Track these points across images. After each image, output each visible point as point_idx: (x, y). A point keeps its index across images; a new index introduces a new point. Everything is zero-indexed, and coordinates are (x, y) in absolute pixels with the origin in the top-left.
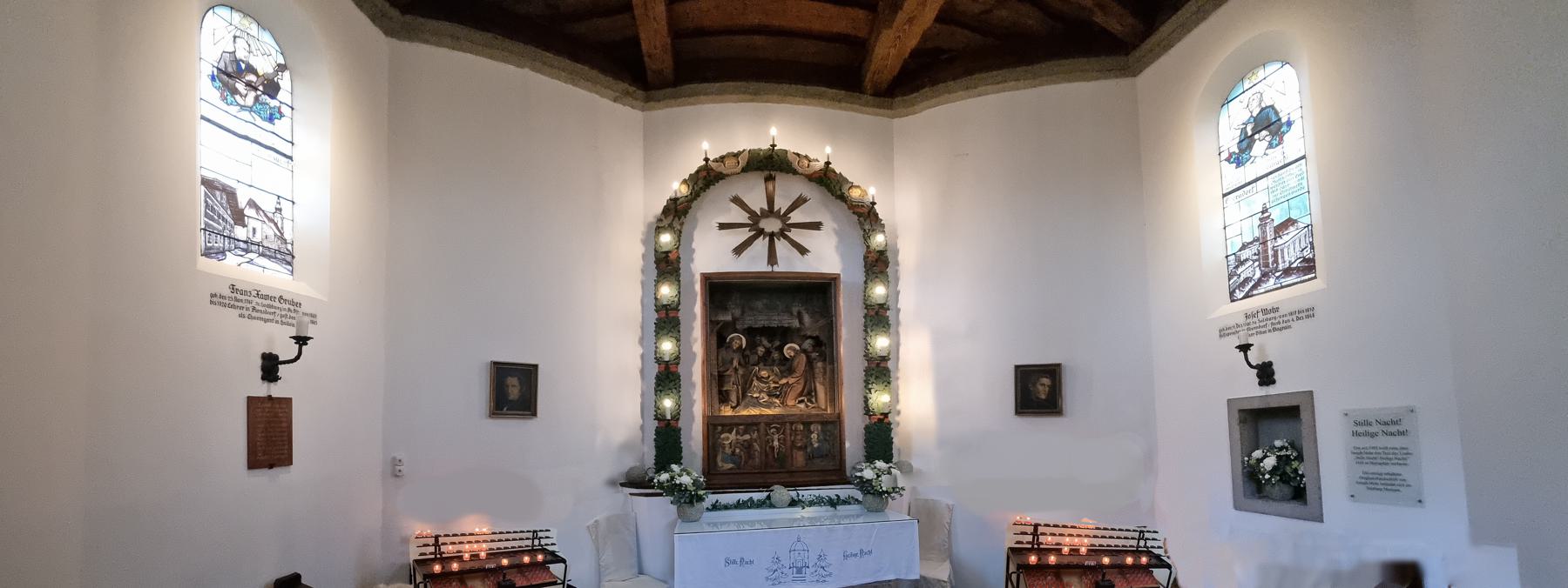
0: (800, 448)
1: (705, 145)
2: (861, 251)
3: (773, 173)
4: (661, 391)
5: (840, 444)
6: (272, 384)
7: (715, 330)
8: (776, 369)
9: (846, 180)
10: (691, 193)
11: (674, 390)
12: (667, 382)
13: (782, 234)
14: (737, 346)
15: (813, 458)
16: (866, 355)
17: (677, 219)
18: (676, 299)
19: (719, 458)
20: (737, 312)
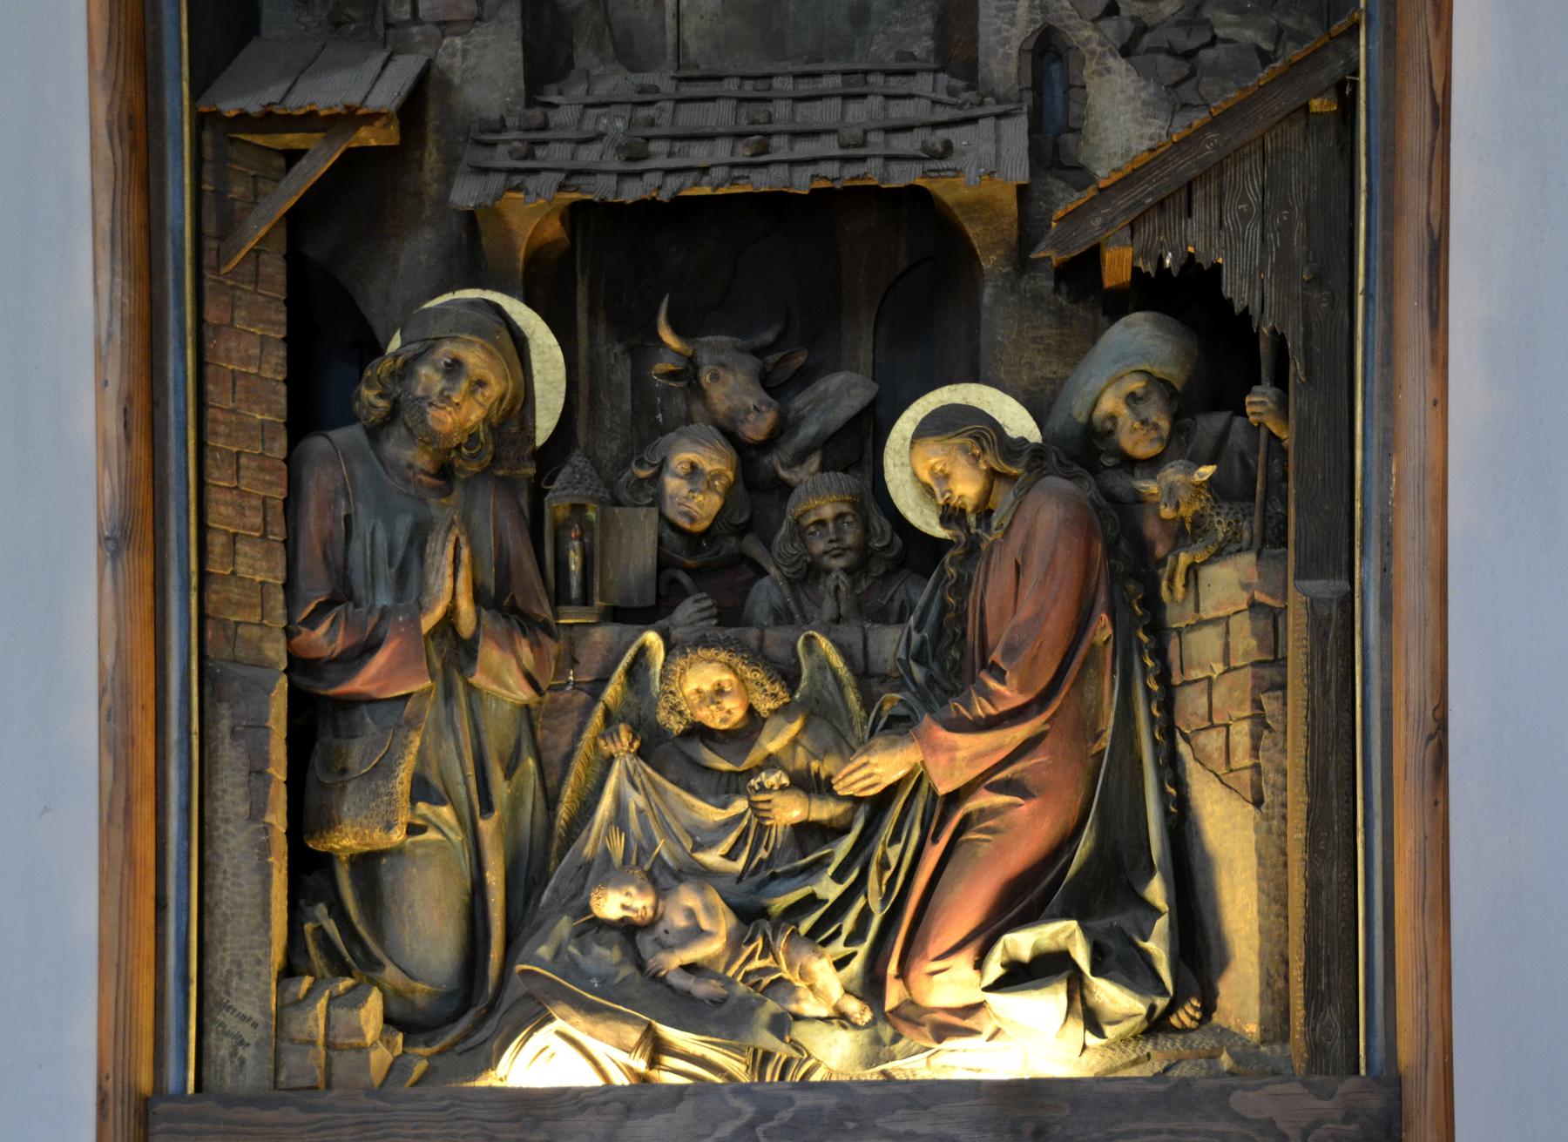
6: (1026, 436)
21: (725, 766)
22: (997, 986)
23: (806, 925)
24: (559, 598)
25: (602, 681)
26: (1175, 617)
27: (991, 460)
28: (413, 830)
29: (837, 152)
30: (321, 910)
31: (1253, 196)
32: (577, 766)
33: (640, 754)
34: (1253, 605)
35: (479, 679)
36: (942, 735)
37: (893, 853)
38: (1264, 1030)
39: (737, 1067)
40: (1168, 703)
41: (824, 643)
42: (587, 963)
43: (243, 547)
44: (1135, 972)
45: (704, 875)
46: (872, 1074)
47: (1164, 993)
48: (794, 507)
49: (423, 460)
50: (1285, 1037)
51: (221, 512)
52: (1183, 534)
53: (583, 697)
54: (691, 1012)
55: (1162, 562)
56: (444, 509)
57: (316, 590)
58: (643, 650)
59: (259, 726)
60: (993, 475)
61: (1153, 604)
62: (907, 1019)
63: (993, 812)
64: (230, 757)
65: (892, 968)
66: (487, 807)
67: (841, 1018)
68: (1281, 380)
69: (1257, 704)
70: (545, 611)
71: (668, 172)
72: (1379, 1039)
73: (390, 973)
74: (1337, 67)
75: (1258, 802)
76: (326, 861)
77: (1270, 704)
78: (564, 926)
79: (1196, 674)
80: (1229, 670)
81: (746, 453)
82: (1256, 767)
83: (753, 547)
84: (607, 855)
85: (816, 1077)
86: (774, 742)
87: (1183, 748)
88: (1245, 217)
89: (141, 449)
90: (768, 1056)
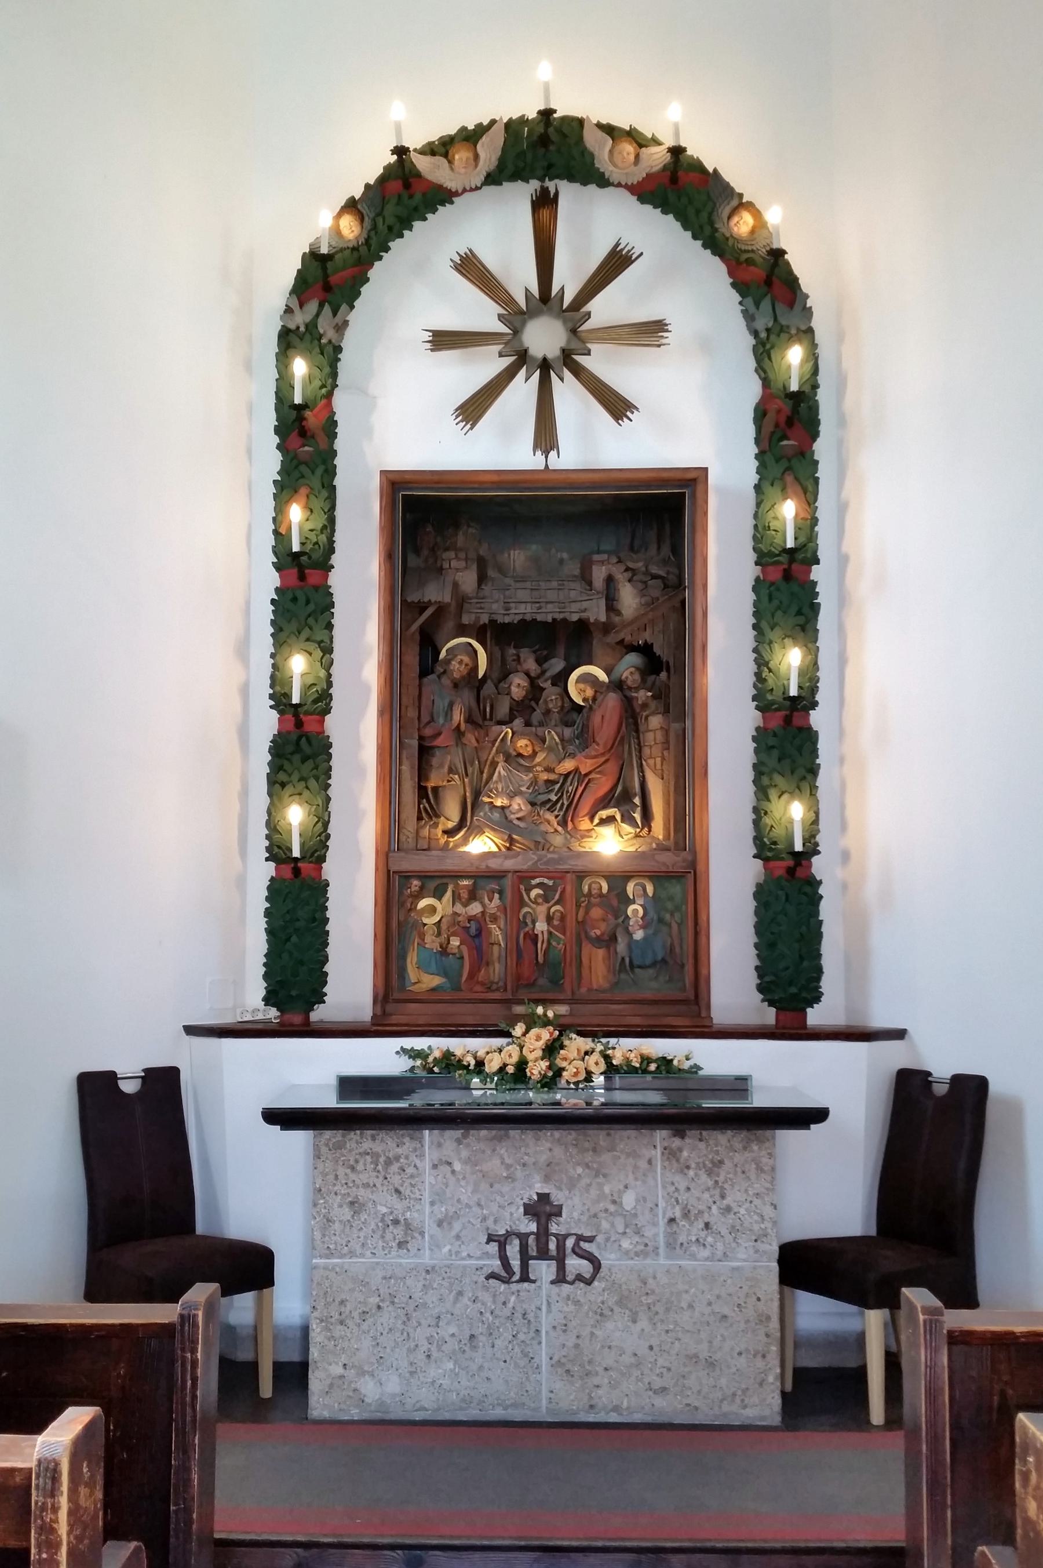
0: (598, 942)
1: (398, 111)
2: (752, 391)
3: (551, 185)
4: (283, 785)
5: (696, 934)
7: (415, 626)
8: (552, 736)
9: (726, 191)
10: (367, 241)
11: (312, 783)
12: (297, 758)
13: (568, 359)
14: (463, 669)
15: (632, 966)
16: (758, 840)
17: (327, 309)
18: (323, 538)
19: (412, 959)
20: (468, 580)
23: (548, 806)
26: (642, 728)
28: (449, 781)
31: (661, 627)
37: (570, 789)
38: (664, 837)
40: (640, 751)
44: (632, 822)
48: (544, 694)
50: (669, 839)
51: (404, 700)
53: (490, 745)
55: (639, 713)
57: (425, 718)
63: (597, 778)
66: (467, 775)
68: (668, 670)
74: (681, 597)
75: (663, 779)
80: (656, 743)
81: (532, 680)
82: (662, 770)
83: (533, 704)
87: (644, 762)
88: (659, 632)
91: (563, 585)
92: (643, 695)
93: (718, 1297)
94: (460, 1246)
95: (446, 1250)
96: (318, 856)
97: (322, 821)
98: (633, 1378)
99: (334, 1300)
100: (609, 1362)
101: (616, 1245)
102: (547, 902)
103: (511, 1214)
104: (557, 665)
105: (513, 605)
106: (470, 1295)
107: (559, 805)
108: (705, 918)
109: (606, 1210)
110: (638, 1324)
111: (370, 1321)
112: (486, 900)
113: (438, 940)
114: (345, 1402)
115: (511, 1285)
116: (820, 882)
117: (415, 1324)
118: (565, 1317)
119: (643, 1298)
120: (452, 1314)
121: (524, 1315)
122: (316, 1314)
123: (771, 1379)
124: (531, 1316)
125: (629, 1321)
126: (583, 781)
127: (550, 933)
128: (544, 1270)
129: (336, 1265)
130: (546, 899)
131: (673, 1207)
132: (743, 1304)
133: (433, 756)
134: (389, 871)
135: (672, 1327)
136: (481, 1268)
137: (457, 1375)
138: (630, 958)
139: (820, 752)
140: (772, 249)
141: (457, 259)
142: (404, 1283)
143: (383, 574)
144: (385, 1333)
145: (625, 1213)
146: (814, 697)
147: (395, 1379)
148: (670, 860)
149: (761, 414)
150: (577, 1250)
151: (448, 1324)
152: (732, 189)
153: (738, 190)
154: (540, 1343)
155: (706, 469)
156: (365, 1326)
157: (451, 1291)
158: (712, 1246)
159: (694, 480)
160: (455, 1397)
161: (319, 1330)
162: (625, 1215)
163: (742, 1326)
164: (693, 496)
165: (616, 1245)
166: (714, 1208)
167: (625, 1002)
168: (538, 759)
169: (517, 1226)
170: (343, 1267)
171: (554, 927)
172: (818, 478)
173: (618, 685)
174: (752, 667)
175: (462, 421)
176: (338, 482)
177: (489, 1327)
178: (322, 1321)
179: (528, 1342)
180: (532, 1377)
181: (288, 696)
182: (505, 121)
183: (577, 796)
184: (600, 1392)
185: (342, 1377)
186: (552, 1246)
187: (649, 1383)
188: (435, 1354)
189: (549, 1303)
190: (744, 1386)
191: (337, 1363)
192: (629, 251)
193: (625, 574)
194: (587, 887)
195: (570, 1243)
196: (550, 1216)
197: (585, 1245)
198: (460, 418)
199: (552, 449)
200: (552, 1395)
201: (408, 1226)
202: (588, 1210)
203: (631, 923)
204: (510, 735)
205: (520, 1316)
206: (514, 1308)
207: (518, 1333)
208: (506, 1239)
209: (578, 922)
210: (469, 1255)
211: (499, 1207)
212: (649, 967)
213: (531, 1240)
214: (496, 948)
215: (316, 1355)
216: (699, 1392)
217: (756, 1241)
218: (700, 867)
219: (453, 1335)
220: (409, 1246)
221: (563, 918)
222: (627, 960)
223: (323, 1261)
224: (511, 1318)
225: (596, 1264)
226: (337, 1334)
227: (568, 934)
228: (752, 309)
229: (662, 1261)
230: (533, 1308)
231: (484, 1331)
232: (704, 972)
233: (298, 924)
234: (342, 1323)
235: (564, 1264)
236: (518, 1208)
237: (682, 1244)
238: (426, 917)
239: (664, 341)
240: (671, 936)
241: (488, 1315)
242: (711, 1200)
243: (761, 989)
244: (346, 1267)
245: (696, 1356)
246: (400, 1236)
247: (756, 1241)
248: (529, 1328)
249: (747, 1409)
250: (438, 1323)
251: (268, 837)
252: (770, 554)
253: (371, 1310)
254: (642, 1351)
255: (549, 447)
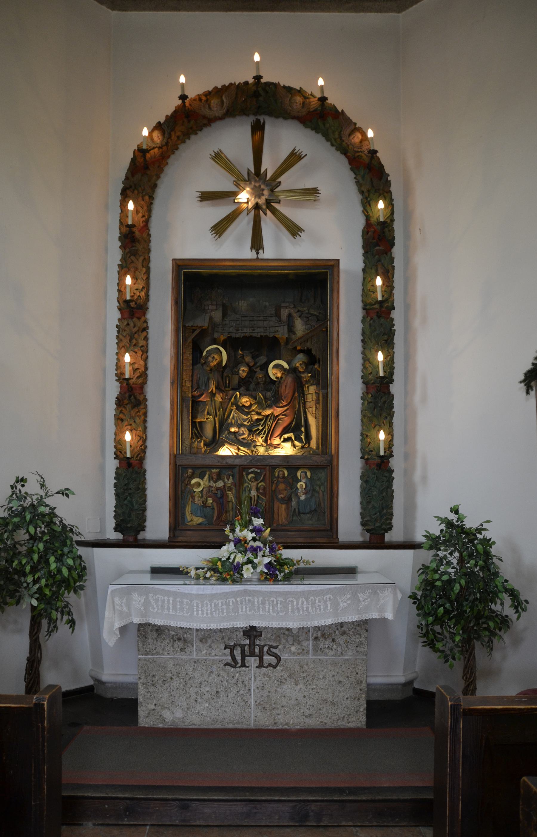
0: (282, 501)
2: (360, 223)
3: (261, 118)
5: (332, 497)
7: (190, 340)
9: (348, 121)
10: (167, 144)
15: (299, 513)
18: (143, 294)
19: (188, 509)
20: (217, 315)
21: (247, 411)
22: (282, 442)
23: (257, 433)
24: (225, 387)
25: (231, 398)
26: (306, 392)
27: (282, 372)
28: (207, 419)
29: (263, 331)
30: (195, 429)
32: (228, 410)
33: (236, 409)
34: (316, 392)
35: (216, 399)
36: (276, 408)
39: (249, 452)
41: (260, 394)
42: (229, 437)
43: (187, 382)
44: (300, 440)
45: (244, 426)
46: (266, 454)
47: (303, 443)
48: (256, 376)
49: (208, 369)
50: (319, 449)
52: (307, 382)
54: (244, 445)
55: (304, 385)
56: (211, 376)
58: (237, 395)
59: (189, 406)
60: (282, 374)
61: (303, 391)
62: (271, 446)
63: (282, 418)
64: (185, 409)
65: (269, 439)
66: (216, 416)
67: (262, 445)
68: (319, 363)
69: (316, 405)
70: (224, 389)
71: (241, 333)
72: (330, 450)
73: (204, 438)
75: (316, 418)
76: (195, 422)
77: (317, 406)
78: (226, 432)
79: (308, 400)
81: (250, 368)
82: (316, 414)
83: (251, 380)
84: (232, 422)
85: (259, 454)
86: (253, 408)
87: (306, 410)
89: (176, 370)
90: (253, 451)
91: (266, 318)
92: (306, 376)
93: (338, 673)
94: (211, 650)
95: (204, 652)
96: (141, 457)
97: (143, 439)
98: (296, 710)
99: (149, 675)
100: (284, 703)
101: (288, 650)
102: (256, 480)
103: (237, 635)
104: (262, 359)
105: (240, 328)
106: (216, 673)
107: (263, 432)
108: (336, 489)
109: (284, 634)
110: (299, 686)
111: (167, 685)
112: (226, 480)
113: (202, 500)
114: (156, 721)
115: (237, 669)
116: (393, 471)
117: (190, 686)
118: (263, 683)
119: (301, 674)
120: (207, 682)
121: (243, 682)
122: (140, 681)
123: (362, 710)
124: (246, 683)
125: (294, 684)
126: (275, 419)
127: (258, 496)
128: (253, 661)
129: (150, 658)
130: (256, 479)
131: (317, 632)
132: (350, 676)
133: (199, 406)
134: (176, 465)
135: (315, 687)
136: (222, 661)
137: (210, 709)
138: (298, 509)
139: (394, 405)
140: (370, 150)
141: (213, 154)
142: (184, 667)
143: (173, 311)
144: (175, 690)
145: (293, 635)
146: (392, 377)
147: (181, 711)
148: (318, 459)
149: (365, 233)
150: (269, 652)
151: (205, 686)
152: (351, 120)
153: (354, 121)
154: (250, 695)
155: (338, 260)
156: (165, 687)
157: (207, 671)
158: (336, 650)
159: (333, 266)
160: (209, 719)
161: (142, 688)
162: (293, 636)
163: (349, 686)
164: (332, 274)
165: (288, 650)
166: (337, 632)
167: (295, 531)
168: (253, 408)
169: (239, 641)
170: (153, 660)
171: (260, 493)
172: (394, 266)
173: (293, 370)
174: (361, 361)
175: (214, 233)
176: (152, 265)
177: (225, 688)
178: (144, 684)
179: (244, 694)
180: (247, 711)
181: (123, 374)
182: (237, 84)
183: (273, 427)
184: (279, 717)
185: (154, 710)
186: (257, 650)
187: (303, 713)
188: (199, 700)
189: (255, 677)
190: (349, 713)
191: (152, 704)
192: (300, 153)
193: (298, 313)
194: (277, 473)
195: (266, 649)
196: (255, 637)
197: (273, 650)
198: (214, 232)
199: (260, 249)
200: (256, 718)
201: (185, 641)
202: (275, 634)
203: (299, 492)
204: (239, 395)
205: (241, 683)
206: (238, 679)
207: (240, 690)
208: (234, 648)
209: (272, 491)
210: (215, 655)
211: (231, 632)
212: (308, 513)
213: (247, 648)
214: (230, 504)
215: (141, 699)
216: (327, 716)
217: (357, 647)
218: (335, 463)
219: (208, 691)
220: (186, 650)
221: (264, 489)
222: (297, 510)
223: (143, 656)
224: (236, 683)
225: (279, 659)
226: (151, 690)
227: (267, 497)
228: (361, 181)
229: (311, 656)
230: (247, 679)
231: (223, 690)
232: (335, 515)
233: (130, 491)
234: (153, 685)
235: (263, 659)
236: (240, 633)
237: (321, 649)
238: (195, 488)
239: (317, 198)
240: (319, 498)
241: (225, 682)
242: (335, 628)
243: (363, 524)
244: (155, 660)
245: (326, 700)
246: (181, 646)
247: (357, 647)
248: (245, 688)
249: (350, 724)
250: (200, 686)
251: (115, 447)
252: (371, 304)
253: (167, 679)
254: (300, 698)
255: (258, 248)
